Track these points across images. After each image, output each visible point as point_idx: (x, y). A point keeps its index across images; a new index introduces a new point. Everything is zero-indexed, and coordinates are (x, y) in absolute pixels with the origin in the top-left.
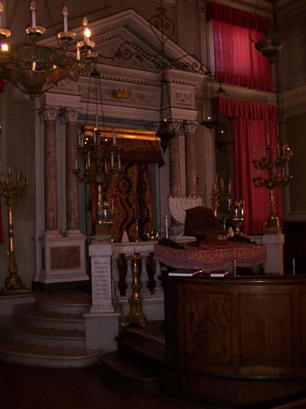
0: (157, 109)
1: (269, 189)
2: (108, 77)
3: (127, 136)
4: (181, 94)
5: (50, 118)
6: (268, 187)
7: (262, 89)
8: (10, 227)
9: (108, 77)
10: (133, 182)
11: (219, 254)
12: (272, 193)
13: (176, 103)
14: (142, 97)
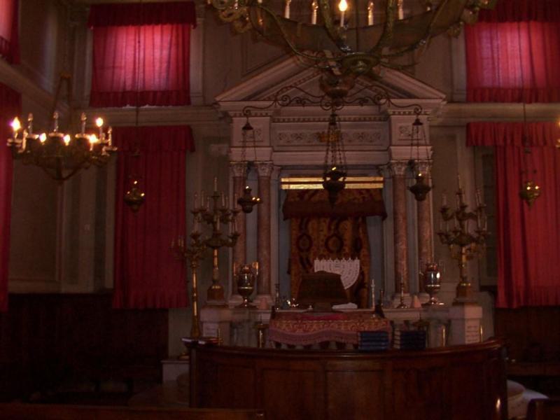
1: (210, 249)
2: (267, 114)
3: (292, 187)
5: (237, 175)
8: (194, 290)
14: (361, 136)
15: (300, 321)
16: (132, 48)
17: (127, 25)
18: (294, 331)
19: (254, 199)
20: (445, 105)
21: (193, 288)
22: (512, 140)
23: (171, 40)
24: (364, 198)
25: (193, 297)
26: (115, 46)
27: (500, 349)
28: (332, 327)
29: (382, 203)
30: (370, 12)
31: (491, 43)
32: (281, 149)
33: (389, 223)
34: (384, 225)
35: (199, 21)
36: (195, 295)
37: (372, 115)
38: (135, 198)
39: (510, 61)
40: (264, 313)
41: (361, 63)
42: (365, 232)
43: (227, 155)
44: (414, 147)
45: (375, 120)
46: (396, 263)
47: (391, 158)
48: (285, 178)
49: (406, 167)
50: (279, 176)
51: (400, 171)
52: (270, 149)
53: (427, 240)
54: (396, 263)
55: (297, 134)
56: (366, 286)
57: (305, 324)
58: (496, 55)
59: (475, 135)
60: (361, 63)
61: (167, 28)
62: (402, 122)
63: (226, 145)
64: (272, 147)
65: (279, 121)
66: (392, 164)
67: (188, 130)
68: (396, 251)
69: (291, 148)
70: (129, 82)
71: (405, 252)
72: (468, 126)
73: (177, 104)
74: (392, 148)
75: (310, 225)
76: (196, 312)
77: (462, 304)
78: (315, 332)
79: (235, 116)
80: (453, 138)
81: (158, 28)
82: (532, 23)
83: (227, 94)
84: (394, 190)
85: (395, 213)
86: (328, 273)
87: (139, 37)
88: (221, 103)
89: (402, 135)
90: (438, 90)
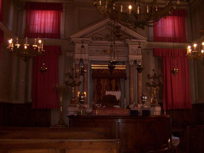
0: (126, 56)
4: (134, 49)
5: (77, 63)
6: (71, 86)
7: (180, 42)
9: (123, 46)
10: (113, 86)
12: (73, 89)
13: (132, 53)
15: (104, 110)
16: (40, 18)
18: (102, 113)
19: (85, 71)
20: (147, 42)
21: (61, 102)
22: (168, 55)
23: (54, 16)
24: (119, 72)
25: (61, 105)
26: (34, 17)
27: (169, 118)
28: (114, 112)
29: (125, 74)
30: (138, 10)
31: (162, 23)
32: (91, 55)
33: (127, 81)
34: (126, 82)
35: (64, 10)
36: (61, 104)
38: (44, 70)
39: (168, 29)
40: (89, 109)
41: (141, 24)
42: (120, 84)
43: (73, 57)
44: (138, 56)
45: (123, 46)
46: (130, 94)
47: (128, 58)
48: (93, 65)
49: (134, 62)
50: (90, 64)
51: (132, 63)
52: (88, 55)
54: (130, 94)
55: (97, 50)
56: (120, 102)
57: (105, 111)
58: (163, 26)
59: (156, 52)
60: (141, 24)
61: (53, 12)
62: (133, 47)
63: (72, 53)
64: (89, 54)
65: (91, 45)
66: (129, 61)
67: (60, 47)
68: (130, 90)
69: (95, 55)
71: (133, 91)
72: (154, 49)
73: (55, 38)
74: (129, 55)
75: (101, 81)
76: (61, 110)
77: (154, 106)
78: (109, 114)
79: (76, 43)
80: (149, 53)
81: (49, 12)
82: (175, 16)
83: (73, 36)
84: (130, 70)
85: (130, 77)
86: (112, 95)
87: (46, 15)
88: (72, 38)
89: (132, 51)
90: (145, 37)
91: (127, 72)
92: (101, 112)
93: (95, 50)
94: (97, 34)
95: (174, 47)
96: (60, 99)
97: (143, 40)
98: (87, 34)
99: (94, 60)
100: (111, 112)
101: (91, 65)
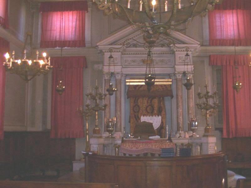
0: (171, 66)
1: (94, 111)
3: (131, 84)
5: (106, 78)
8: (87, 130)
11: (140, 146)
15: (134, 144)
16: (59, 22)
17: (67, 11)
18: (132, 148)
20: (199, 47)
21: (87, 129)
22: (230, 63)
23: (77, 18)
24: (163, 89)
25: (87, 133)
27: (224, 156)
28: (149, 146)
29: (171, 91)
33: (174, 100)
34: (172, 101)
35: (89, 9)
36: (87, 132)
37: (167, 51)
38: (60, 89)
39: (229, 27)
41: (162, 28)
42: (164, 104)
43: (102, 69)
44: (185, 66)
45: (168, 54)
46: (177, 118)
47: (175, 71)
48: (128, 79)
49: (182, 75)
50: (125, 79)
52: (121, 67)
53: (191, 108)
54: (177, 118)
55: (133, 60)
56: (164, 128)
57: (137, 145)
58: (222, 25)
59: (213, 60)
60: (162, 28)
61: (75, 12)
62: (180, 55)
63: (101, 65)
65: (125, 54)
66: (176, 73)
67: (85, 58)
68: (177, 113)
70: (58, 37)
71: (182, 113)
72: (210, 56)
73: (79, 47)
74: (176, 66)
76: (88, 139)
77: (207, 136)
78: (141, 149)
79: (105, 52)
80: (203, 62)
81: (71, 13)
84: (177, 85)
85: (177, 95)
89: (180, 60)
90: (196, 40)
91: (174, 87)
92: (131, 146)
93: (131, 61)
94: (132, 40)
95: (235, 52)
96: (86, 125)
97: (194, 45)
98: (119, 40)
99: (130, 73)
100: (144, 146)
101: (126, 80)
